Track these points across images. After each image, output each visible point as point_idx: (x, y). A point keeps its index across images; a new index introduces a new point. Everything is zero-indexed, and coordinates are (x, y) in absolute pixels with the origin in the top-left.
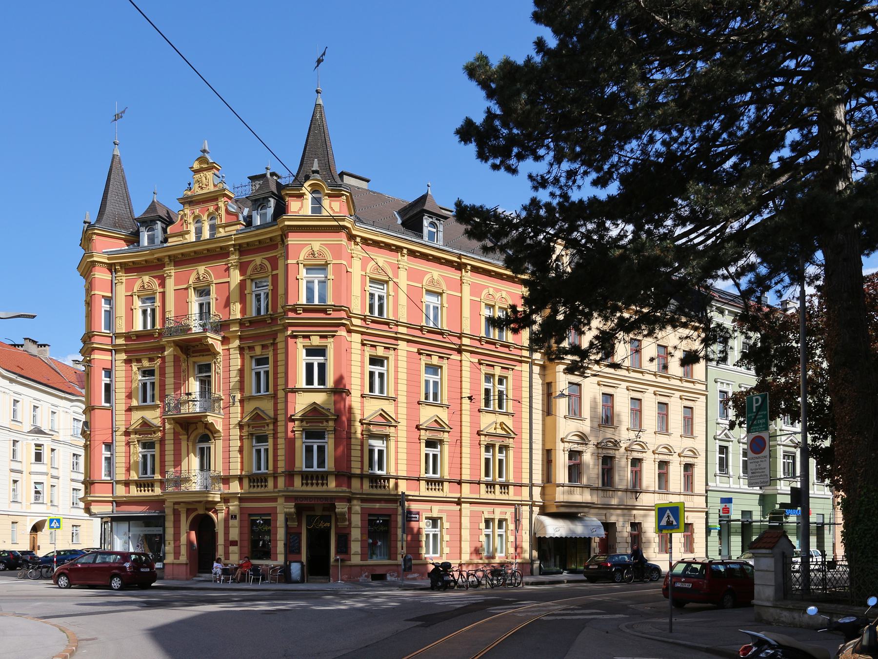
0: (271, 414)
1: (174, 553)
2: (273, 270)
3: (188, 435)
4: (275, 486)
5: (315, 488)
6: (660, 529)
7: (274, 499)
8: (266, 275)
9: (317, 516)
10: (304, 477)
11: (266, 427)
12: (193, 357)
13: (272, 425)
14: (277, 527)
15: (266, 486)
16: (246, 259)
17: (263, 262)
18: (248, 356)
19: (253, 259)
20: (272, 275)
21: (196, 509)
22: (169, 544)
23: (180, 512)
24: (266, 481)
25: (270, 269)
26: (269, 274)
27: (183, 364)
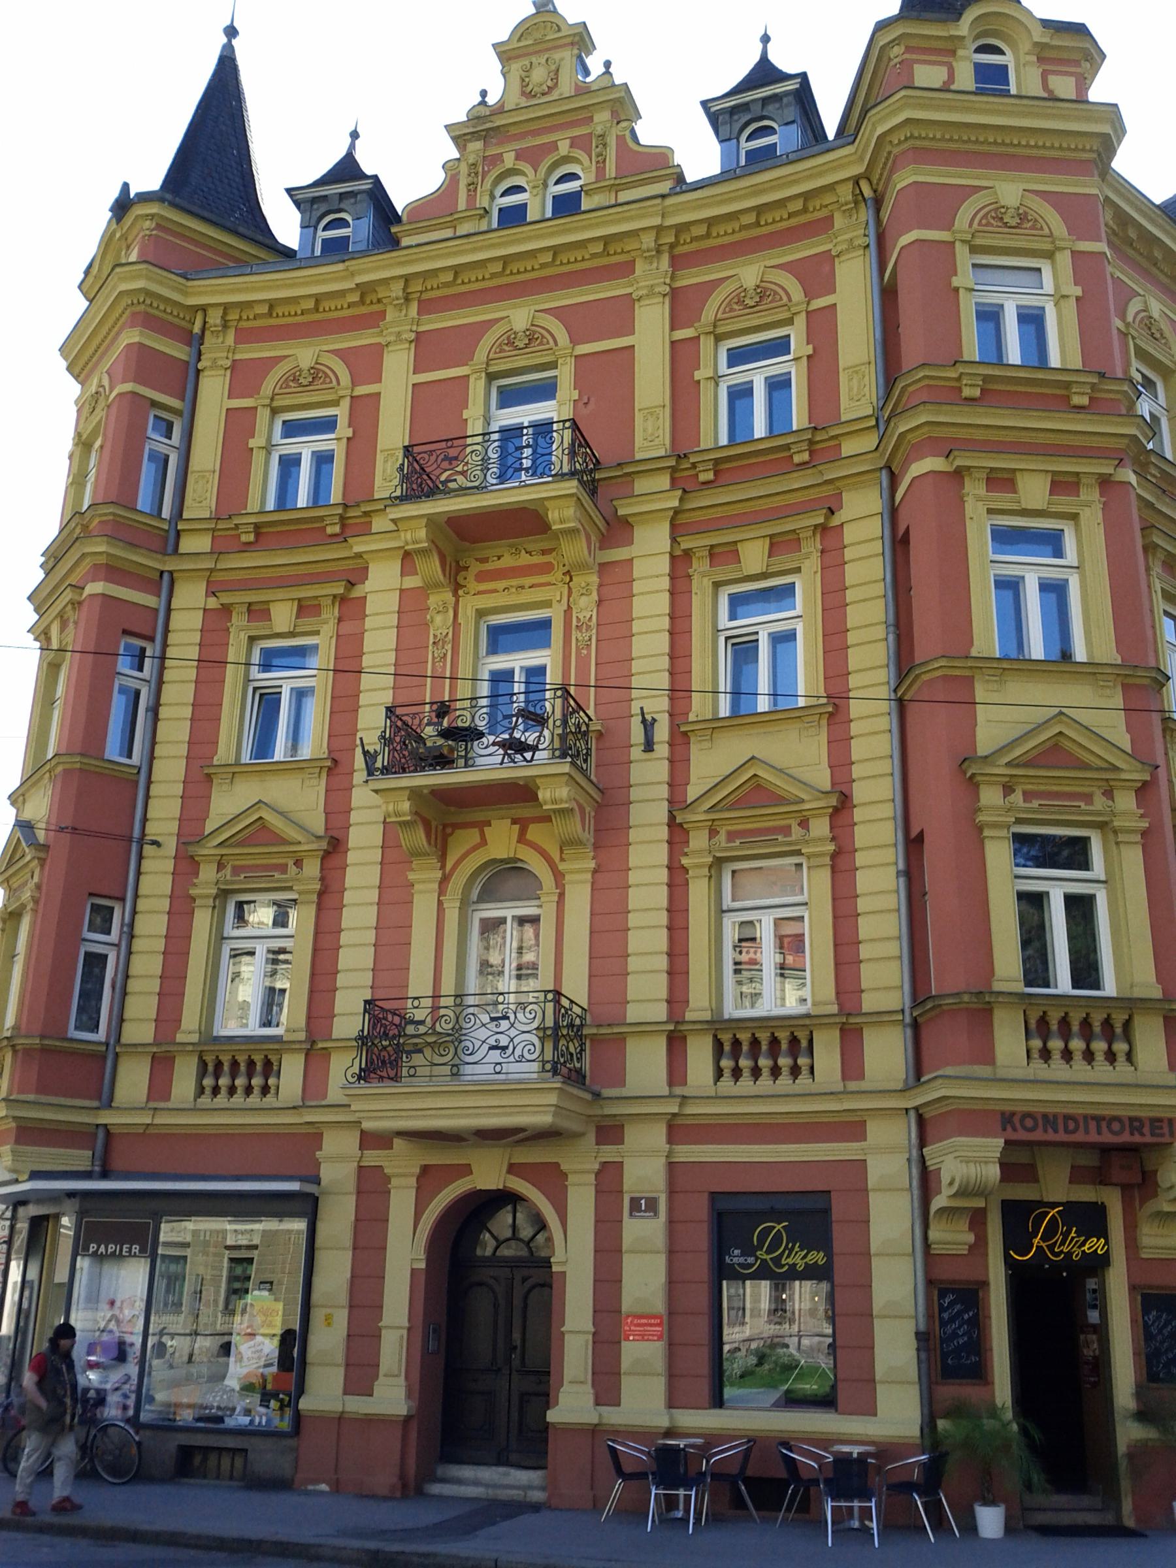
0: (823, 779)
1: (347, 1365)
2: (810, 295)
3: (443, 867)
4: (852, 1066)
5: (1080, 1070)
6: (181, 1304)
7: (854, 1129)
8: (786, 315)
9: (1053, 1205)
10: (727, 1048)
11: (292, 869)
12: (479, 593)
13: (826, 821)
14: (867, 1255)
15: (265, 1090)
16: (691, 278)
17: (767, 277)
18: (707, 583)
19: (286, 353)
20: (808, 313)
21: (466, 1170)
22: (328, 1320)
23: (387, 1179)
24: (269, 1068)
25: (345, 378)
26: (341, 393)
27: (438, 619)
